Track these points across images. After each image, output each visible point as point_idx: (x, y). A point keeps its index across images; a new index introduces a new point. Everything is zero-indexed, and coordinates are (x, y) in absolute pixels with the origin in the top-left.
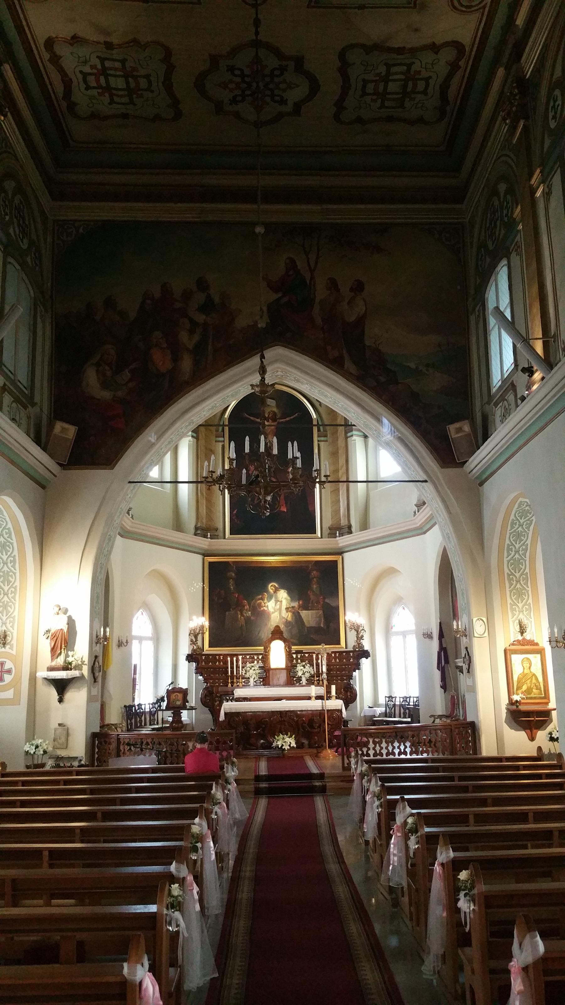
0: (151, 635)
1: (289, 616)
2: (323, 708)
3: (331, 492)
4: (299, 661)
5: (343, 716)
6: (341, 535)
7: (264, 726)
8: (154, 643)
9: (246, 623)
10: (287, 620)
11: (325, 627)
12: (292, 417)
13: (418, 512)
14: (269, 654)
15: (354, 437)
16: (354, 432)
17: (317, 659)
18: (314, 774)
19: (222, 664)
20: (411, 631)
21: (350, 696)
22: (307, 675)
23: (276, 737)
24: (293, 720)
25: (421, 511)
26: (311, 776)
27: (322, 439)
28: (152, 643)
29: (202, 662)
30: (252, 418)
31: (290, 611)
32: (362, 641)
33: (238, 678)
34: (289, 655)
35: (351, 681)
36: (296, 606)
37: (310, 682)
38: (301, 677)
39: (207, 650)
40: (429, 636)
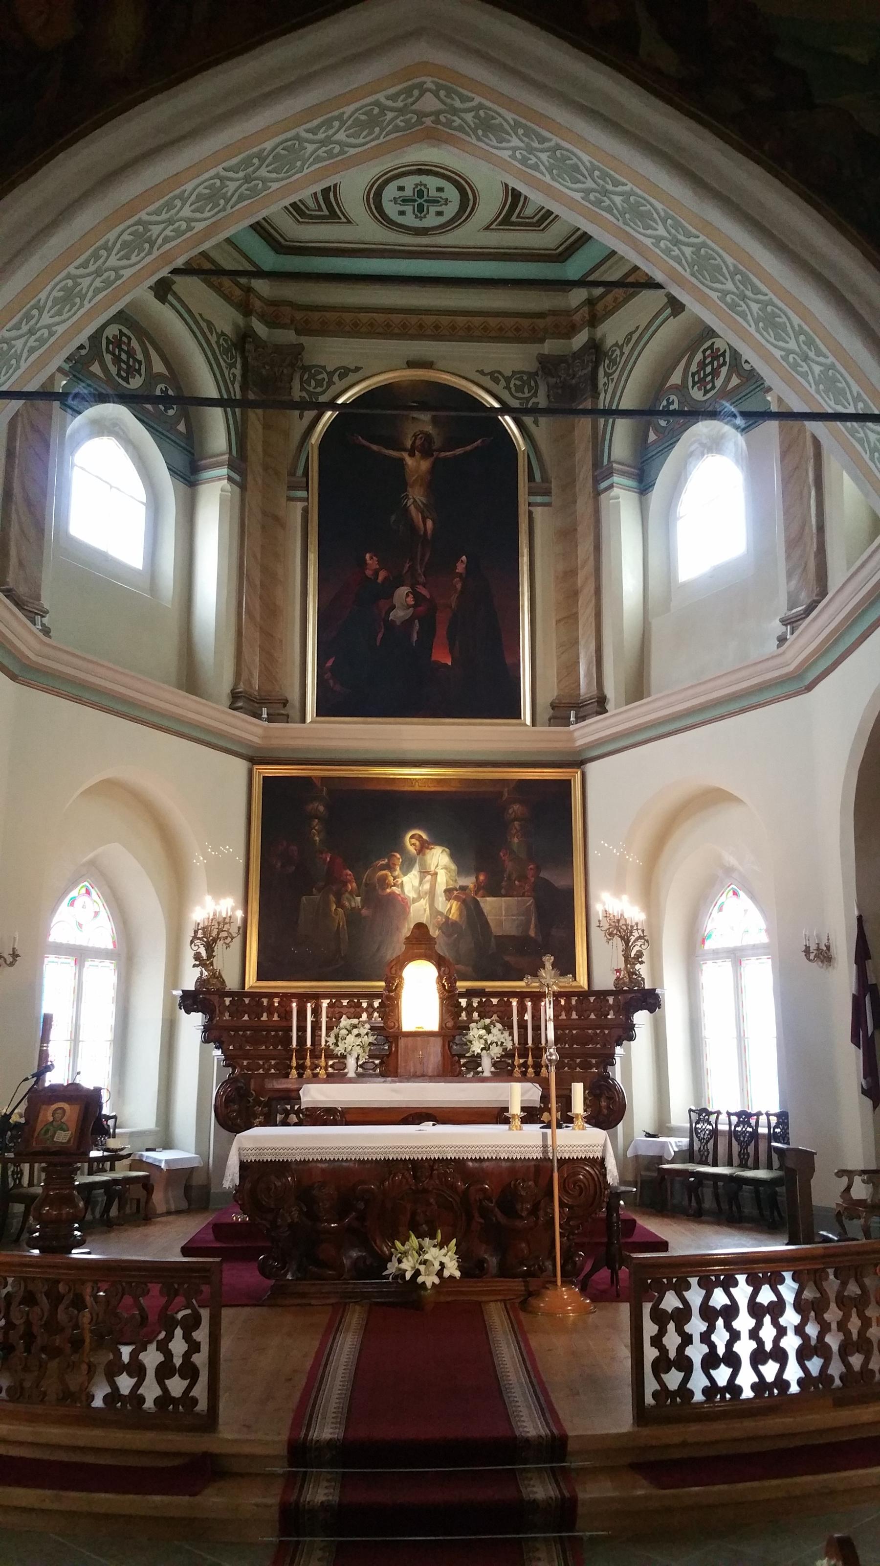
0: (111, 946)
1: (452, 909)
2: (545, 1152)
3: (558, 622)
4: (475, 1015)
5: (610, 1180)
6: (580, 718)
7: (361, 1205)
8: (118, 968)
9: (349, 922)
10: (447, 918)
11: (540, 939)
12: (469, 448)
13: (792, 633)
14: (398, 997)
15: (616, 491)
16: (616, 479)
17: (522, 1010)
18: (527, 1440)
19: (276, 1018)
20: (754, 947)
21: (608, 1107)
22: (496, 1051)
23: (398, 1244)
24: (453, 1187)
25: (796, 633)
26: (511, 1450)
27: (539, 499)
28: (112, 966)
29: (222, 1014)
30: (375, 447)
31: (457, 898)
32: (638, 967)
33: (315, 1055)
34: (448, 998)
35: (609, 1068)
36: (472, 886)
37: (504, 1070)
38: (479, 1056)
39: (251, 987)
40: (823, 955)
